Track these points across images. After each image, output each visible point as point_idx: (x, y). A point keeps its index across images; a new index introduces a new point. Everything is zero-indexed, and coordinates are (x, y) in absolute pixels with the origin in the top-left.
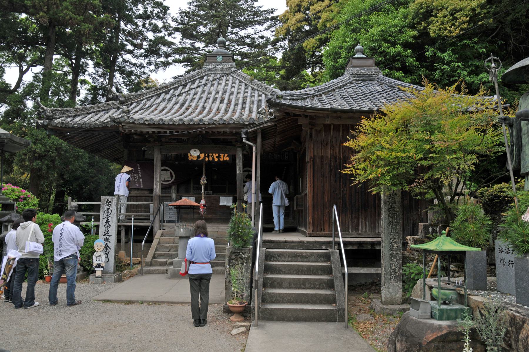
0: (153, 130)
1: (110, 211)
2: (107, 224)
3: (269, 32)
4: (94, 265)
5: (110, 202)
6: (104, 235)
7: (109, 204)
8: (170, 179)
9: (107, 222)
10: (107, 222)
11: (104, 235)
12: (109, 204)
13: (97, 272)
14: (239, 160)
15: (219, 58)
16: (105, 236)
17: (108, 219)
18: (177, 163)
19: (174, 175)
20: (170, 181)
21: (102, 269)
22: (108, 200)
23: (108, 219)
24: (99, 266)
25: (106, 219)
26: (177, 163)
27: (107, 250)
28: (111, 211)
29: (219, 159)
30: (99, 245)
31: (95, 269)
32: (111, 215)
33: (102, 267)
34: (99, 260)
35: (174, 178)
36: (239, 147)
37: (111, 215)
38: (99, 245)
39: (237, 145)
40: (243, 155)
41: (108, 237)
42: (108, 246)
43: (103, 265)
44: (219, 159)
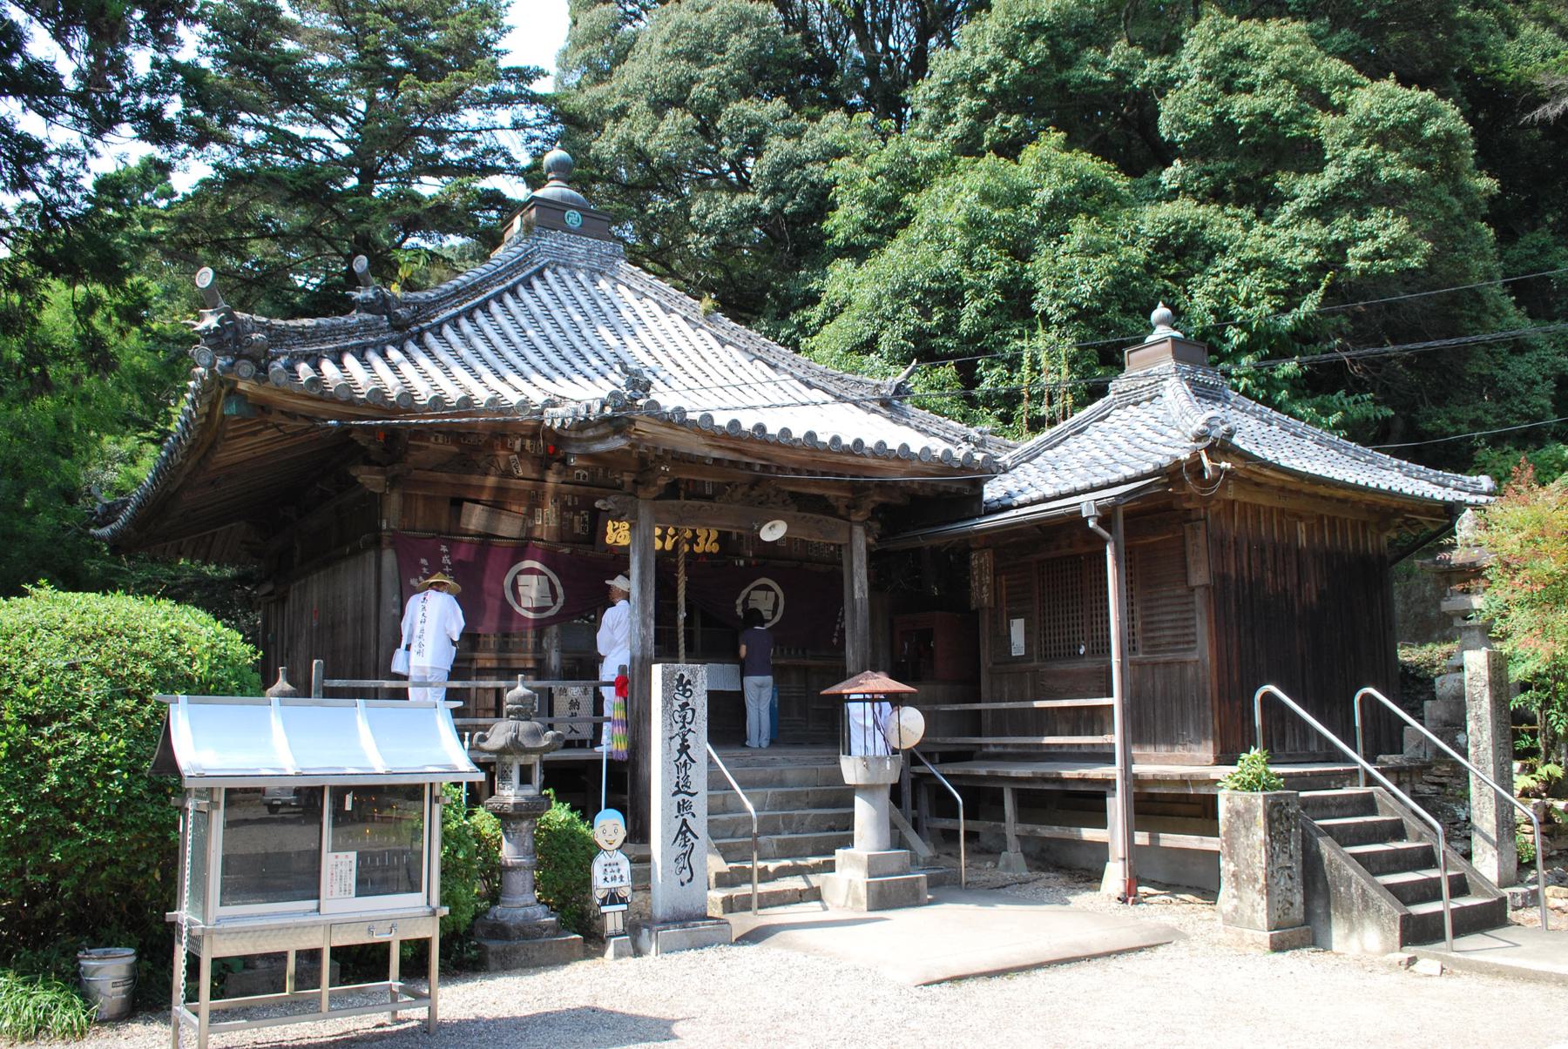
0: (716, 454)
1: (690, 713)
2: (684, 757)
3: (519, 137)
4: (599, 895)
5: (689, 682)
6: (675, 794)
7: (685, 691)
8: (771, 594)
9: (684, 748)
10: (684, 748)
11: (675, 794)
12: (685, 691)
13: (609, 918)
15: (573, 218)
16: (680, 797)
17: (684, 740)
18: (567, 551)
19: (560, 590)
20: (777, 596)
21: (624, 907)
22: (682, 676)
23: (684, 740)
24: (613, 898)
25: (678, 740)
26: (567, 551)
27: (686, 840)
29: (691, 548)
30: (610, 830)
31: (604, 909)
32: (692, 727)
33: (623, 901)
34: (614, 879)
35: (561, 600)
36: (860, 523)
37: (692, 727)
38: (610, 830)
39: (853, 518)
40: (868, 546)
42: (689, 829)
43: (626, 892)
44: (691, 548)
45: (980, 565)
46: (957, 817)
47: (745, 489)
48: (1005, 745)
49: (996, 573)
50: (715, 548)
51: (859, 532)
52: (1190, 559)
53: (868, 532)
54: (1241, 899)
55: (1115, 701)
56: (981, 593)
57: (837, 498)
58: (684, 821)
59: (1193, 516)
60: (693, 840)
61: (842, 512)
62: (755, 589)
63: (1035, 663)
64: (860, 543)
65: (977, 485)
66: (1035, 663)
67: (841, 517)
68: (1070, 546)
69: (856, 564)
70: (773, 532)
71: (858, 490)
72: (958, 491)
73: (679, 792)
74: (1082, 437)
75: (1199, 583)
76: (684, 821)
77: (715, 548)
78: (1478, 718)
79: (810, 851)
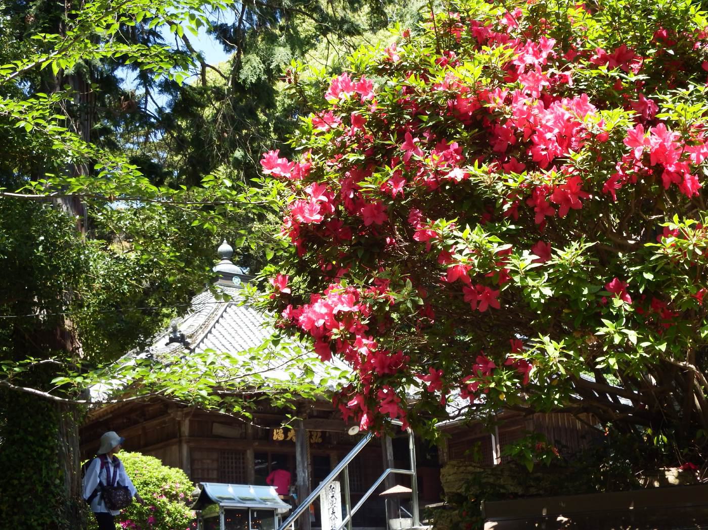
25: (331, 510)
50: (320, 440)
77: (320, 440)
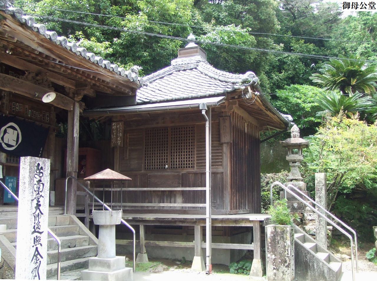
0: (40, 50)
6: (33, 233)
8: (16, 132)
9: (38, 205)
10: (38, 205)
11: (33, 233)
14: (77, 119)
22: (39, 164)
23: (39, 201)
25: (35, 202)
28: (43, 184)
36: (78, 102)
40: (80, 113)
41: (38, 235)
42: (39, 254)
45: (117, 129)
46: (133, 239)
47: (34, 75)
48: (135, 207)
49: (125, 132)
51: (77, 105)
52: (222, 132)
53: (80, 106)
54: (278, 270)
55: (208, 189)
56: (117, 140)
57: (70, 88)
58: (37, 248)
59: (224, 115)
60: (41, 259)
61: (71, 95)
62: (8, 127)
63: (143, 171)
64: (78, 112)
65: (134, 90)
66: (143, 171)
67: (70, 97)
68: (164, 123)
69: (75, 120)
70: (49, 98)
71: (80, 85)
72: (126, 93)
73: (35, 232)
74: (163, 80)
75: (226, 141)
76: (37, 248)
78: (320, 197)
79: (251, 264)
